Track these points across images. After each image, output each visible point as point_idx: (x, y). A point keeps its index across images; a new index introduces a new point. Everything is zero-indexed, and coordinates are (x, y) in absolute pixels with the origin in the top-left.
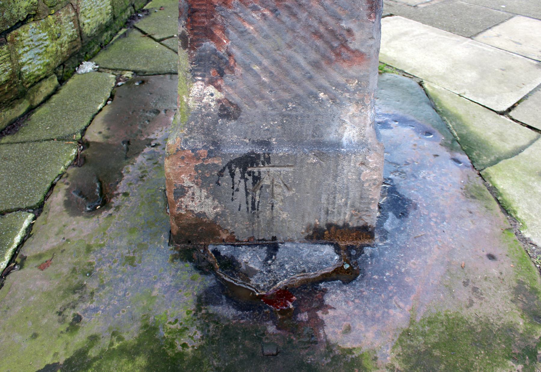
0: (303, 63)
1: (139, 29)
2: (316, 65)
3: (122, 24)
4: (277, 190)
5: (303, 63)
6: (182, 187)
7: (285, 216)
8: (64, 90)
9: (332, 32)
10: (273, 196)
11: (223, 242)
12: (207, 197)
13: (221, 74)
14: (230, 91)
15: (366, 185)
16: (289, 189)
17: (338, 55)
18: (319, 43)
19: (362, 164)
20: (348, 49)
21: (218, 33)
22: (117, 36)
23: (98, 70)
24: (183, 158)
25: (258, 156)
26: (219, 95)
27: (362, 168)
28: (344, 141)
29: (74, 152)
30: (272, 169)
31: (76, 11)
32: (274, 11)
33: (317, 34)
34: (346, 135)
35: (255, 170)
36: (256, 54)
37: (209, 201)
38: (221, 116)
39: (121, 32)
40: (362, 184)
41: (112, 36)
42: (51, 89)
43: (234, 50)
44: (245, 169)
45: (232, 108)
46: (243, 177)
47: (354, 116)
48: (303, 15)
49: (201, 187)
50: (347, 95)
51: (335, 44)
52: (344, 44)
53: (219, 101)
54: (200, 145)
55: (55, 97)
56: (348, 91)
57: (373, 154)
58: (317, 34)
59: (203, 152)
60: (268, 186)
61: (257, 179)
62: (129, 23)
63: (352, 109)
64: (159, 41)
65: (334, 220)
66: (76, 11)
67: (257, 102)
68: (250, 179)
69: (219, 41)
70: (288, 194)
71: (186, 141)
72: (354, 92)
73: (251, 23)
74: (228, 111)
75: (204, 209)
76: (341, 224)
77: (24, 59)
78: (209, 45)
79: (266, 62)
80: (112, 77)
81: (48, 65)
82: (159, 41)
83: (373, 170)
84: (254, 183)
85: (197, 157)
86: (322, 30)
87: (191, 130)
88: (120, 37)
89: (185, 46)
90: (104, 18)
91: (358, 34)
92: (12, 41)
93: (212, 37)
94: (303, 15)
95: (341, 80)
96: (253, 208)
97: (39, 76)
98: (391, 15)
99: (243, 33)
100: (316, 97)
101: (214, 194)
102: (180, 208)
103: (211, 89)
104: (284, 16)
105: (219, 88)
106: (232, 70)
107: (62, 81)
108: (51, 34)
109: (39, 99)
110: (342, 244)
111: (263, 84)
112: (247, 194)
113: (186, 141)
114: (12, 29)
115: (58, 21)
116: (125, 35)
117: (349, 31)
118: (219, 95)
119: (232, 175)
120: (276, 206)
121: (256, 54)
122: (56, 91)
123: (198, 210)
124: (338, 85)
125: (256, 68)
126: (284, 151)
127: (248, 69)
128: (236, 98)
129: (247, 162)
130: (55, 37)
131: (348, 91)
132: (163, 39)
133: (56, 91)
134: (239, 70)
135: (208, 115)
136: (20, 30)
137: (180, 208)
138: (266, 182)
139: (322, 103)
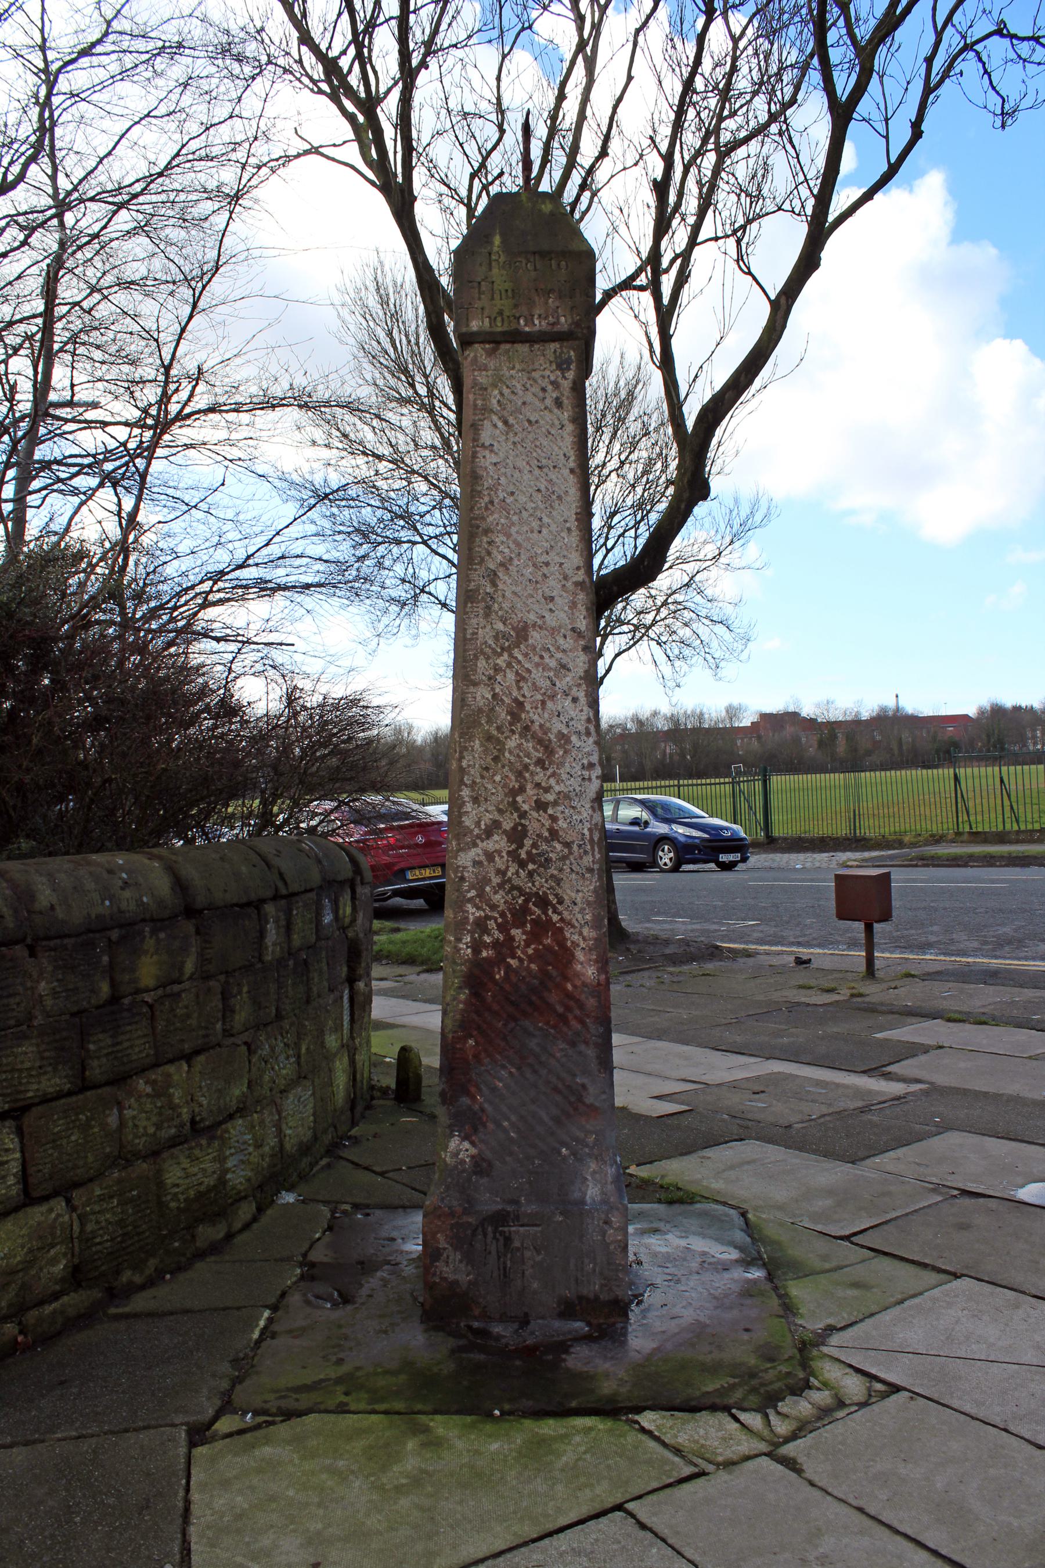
0: (546, 1119)
1: (348, 1160)
2: (557, 1121)
3: (322, 1150)
4: (528, 1254)
5: (546, 1119)
6: (438, 1249)
7: (535, 1285)
8: (265, 1219)
9: (568, 1087)
10: (523, 1263)
11: (476, 1318)
12: (461, 1261)
13: (476, 1130)
14: (483, 1147)
15: (612, 1247)
16: (538, 1253)
17: (576, 1109)
18: (558, 1098)
19: (606, 1223)
20: (584, 1103)
21: (473, 1090)
22: (318, 1167)
23: (303, 1202)
24: (439, 1217)
25: (508, 1212)
26: (473, 1151)
27: (606, 1227)
28: (588, 1199)
29: (299, 1271)
30: (522, 1229)
31: (279, 1113)
32: (519, 1069)
33: (556, 1089)
34: (589, 1193)
35: (506, 1229)
36: (505, 1109)
37: (462, 1266)
38: (475, 1173)
39: (324, 1162)
40: (608, 1245)
41: (312, 1165)
42: (249, 1216)
43: (486, 1106)
44: (496, 1228)
45: (484, 1165)
46: (495, 1238)
47: (594, 1172)
48: (544, 1072)
49: (456, 1249)
50: (587, 1150)
51: (573, 1099)
52: (580, 1099)
53: (473, 1157)
54: (455, 1203)
55: (255, 1226)
56: (587, 1146)
57: (616, 1213)
58: (556, 1089)
59: (459, 1209)
60: (518, 1249)
61: (508, 1240)
62: (333, 1150)
63: (593, 1166)
64: (382, 1174)
65: (585, 1292)
66: (279, 1113)
67: (508, 1159)
68: (502, 1239)
69: (473, 1098)
70: (539, 1258)
71: (443, 1199)
72: (593, 1148)
73: (500, 1080)
74: (480, 1166)
75: (457, 1277)
76: (591, 1296)
77: (229, 1164)
78: (465, 1100)
79: (513, 1118)
80: (325, 1210)
81: (249, 1180)
82: (382, 1174)
83: (616, 1229)
84: (505, 1245)
85: (452, 1214)
86: (560, 1086)
87: (448, 1188)
88: (322, 1168)
89: (444, 1103)
90: (306, 1135)
91: (591, 1089)
92: (221, 1138)
93: (468, 1093)
94: (544, 1072)
95: (580, 1135)
96: (505, 1276)
97: (239, 1192)
98: (741, 1140)
99: (494, 1089)
100: (559, 1153)
101: (468, 1258)
102: (434, 1274)
103: (466, 1145)
104: (529, 1075)
105: (473, 1143)
106: (485, 1126)
107: (260, 1210)
108: (254, 1137)
109: (238, 1225)
110: (595, 1322)
111: (511, 1140)
112: (499, 1258)
113: (443, 1199)
114: (220, 1123)
115: (262, 1122)
116: (329, 1166)
117: (583, 1086)
118: (473, 1151)
119: (485, 1235)
120: (527, 1273)
121: (505, 1109)
122: (255, 1219)
123: (451, 1277)
124: (577, 1140)
125: (506, 1124)
126: (532, 1208)
127: (498, 1125)
128: (488, 1155)
129: (500, 1219)
130: (258, 1146)
131: (587, 1146)
132: (387, 1172)
133: (255, 1219)
134: (491, 1126)
135: (464, 1171)
136: (229, 1125)
137: (434, 1274)
138: (517, 1244)
139: (565, 1158)
